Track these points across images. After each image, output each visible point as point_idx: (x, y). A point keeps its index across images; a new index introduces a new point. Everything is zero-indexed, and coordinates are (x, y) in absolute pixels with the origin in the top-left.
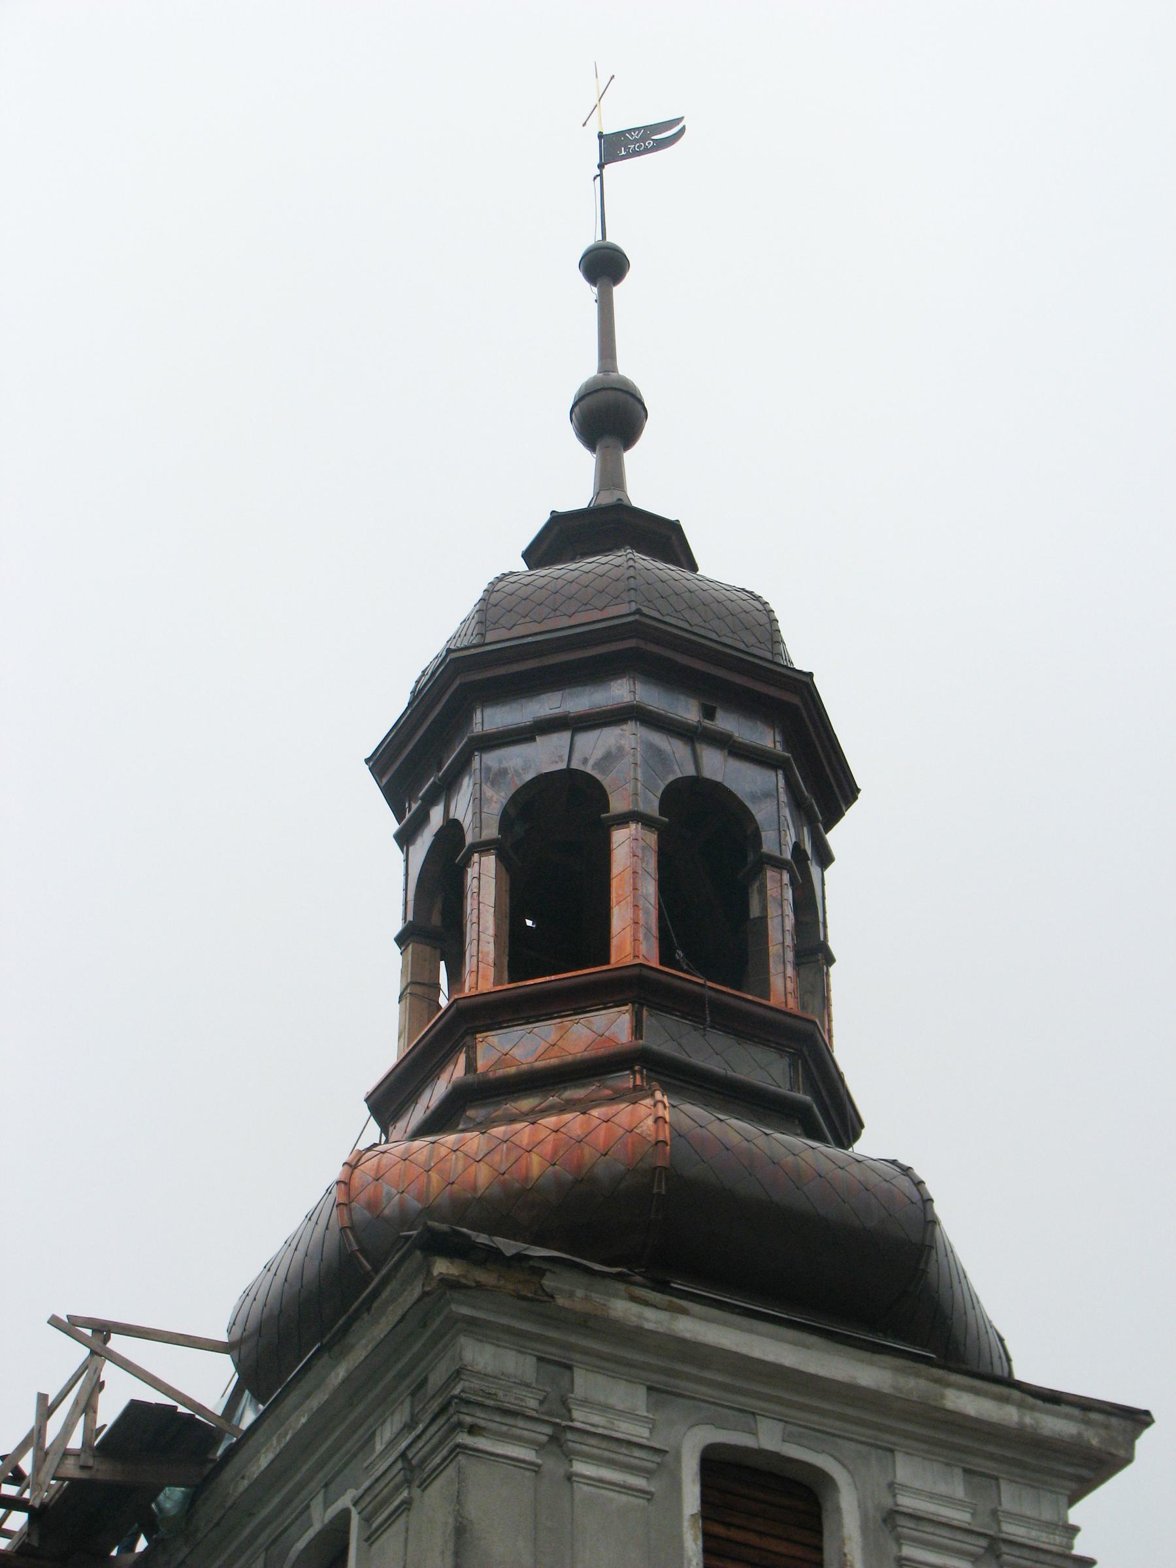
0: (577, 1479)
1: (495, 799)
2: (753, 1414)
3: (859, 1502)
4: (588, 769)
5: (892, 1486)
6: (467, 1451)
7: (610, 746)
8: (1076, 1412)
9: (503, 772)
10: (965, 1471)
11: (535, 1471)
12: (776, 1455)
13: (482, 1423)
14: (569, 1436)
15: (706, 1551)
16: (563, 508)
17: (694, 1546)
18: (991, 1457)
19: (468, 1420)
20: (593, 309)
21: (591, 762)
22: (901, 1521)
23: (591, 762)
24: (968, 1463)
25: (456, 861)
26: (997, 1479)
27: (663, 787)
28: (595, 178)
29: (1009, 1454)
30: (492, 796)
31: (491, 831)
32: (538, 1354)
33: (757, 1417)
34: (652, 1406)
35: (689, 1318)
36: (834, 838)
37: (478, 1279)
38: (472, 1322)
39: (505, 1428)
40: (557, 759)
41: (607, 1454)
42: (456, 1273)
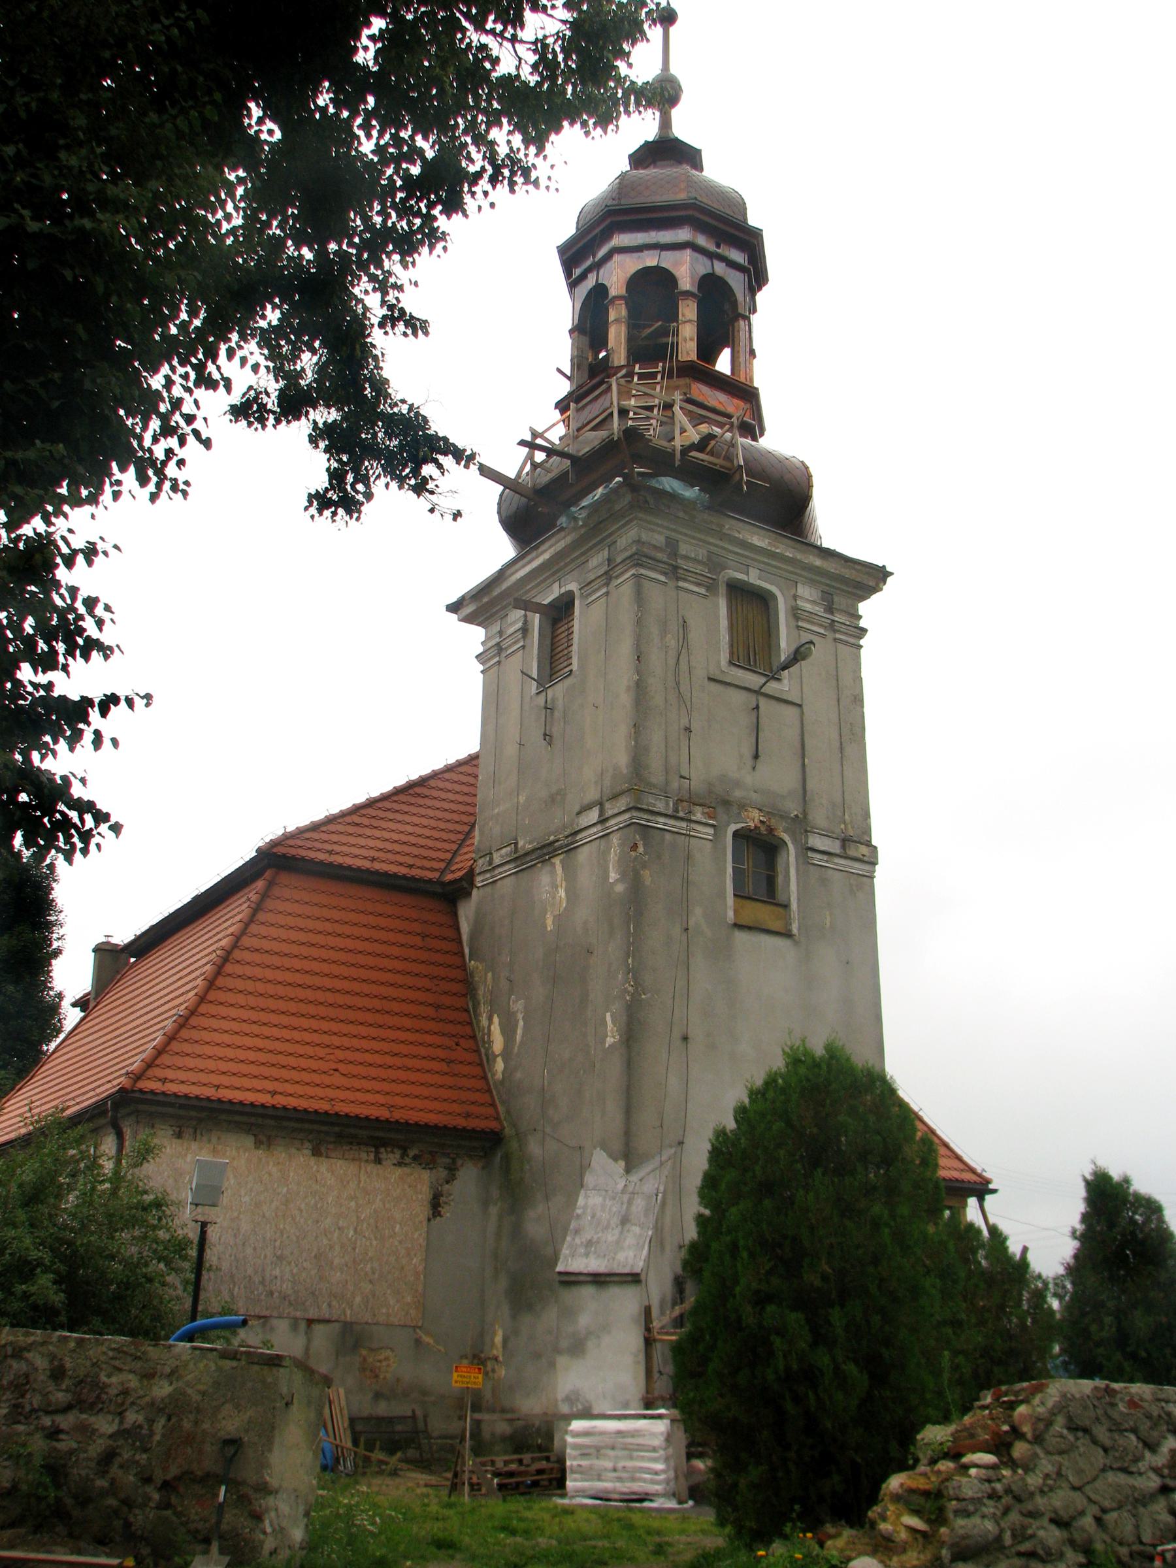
16: (631, 152)
31: (623, 291)
36: (760, 297)
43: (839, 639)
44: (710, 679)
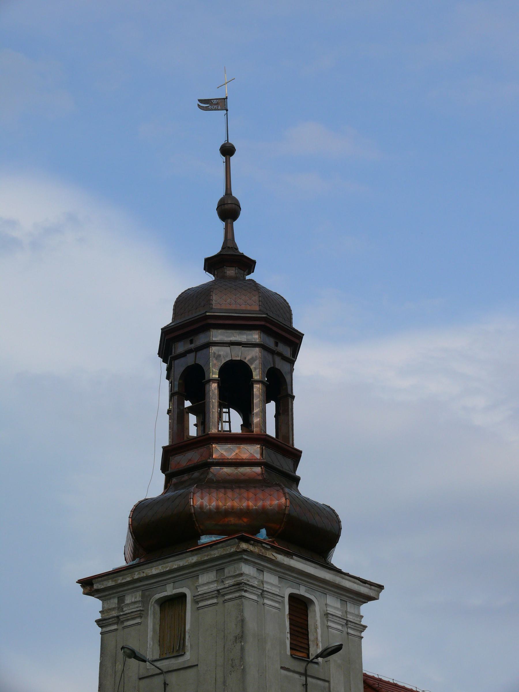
0: (266, 605)
1: (217, 364)
2: (299, 584)
3: (319, 610)
4: (246, 361)
5: (326, 604)
6: (244, 598)
7: (253, 355)
8: (369, 586)
9: (219, 356)
10: (341, 600)
11: (257, 603)
12: (303, 596)
13: (248, 589)
14: (265, 593)
15: (290, 624)
17: (288, 623)
18: (347, 596)
19: (245, 588)
20: (223, 166)
21: (247, 359)
22: (329, 616)
23: (247, 359)
24: (342, 598)
25: (203, 381)
26: (346, 602)
27: (267, 371)
28: (225, 115)
29: (351, 596)
30: (216, 363)
32: (257, 568)
33: (300, 585)
34: (280, 582)
35: (293, 560)
37: (251, 550)
38: (246, 559)
39: (252, 591)
40: (237, 356)
41: (272, 598)
42: (246, 547)
43: (226, 600)
44: (140, 679)
